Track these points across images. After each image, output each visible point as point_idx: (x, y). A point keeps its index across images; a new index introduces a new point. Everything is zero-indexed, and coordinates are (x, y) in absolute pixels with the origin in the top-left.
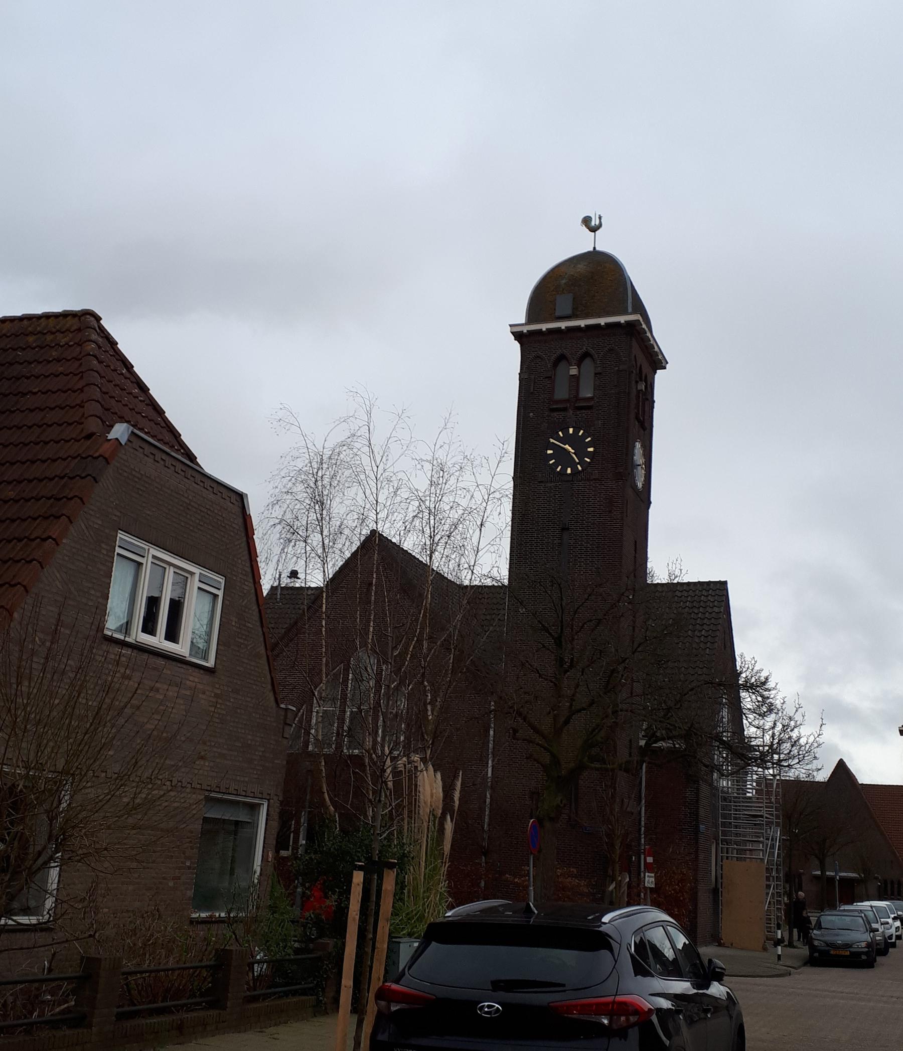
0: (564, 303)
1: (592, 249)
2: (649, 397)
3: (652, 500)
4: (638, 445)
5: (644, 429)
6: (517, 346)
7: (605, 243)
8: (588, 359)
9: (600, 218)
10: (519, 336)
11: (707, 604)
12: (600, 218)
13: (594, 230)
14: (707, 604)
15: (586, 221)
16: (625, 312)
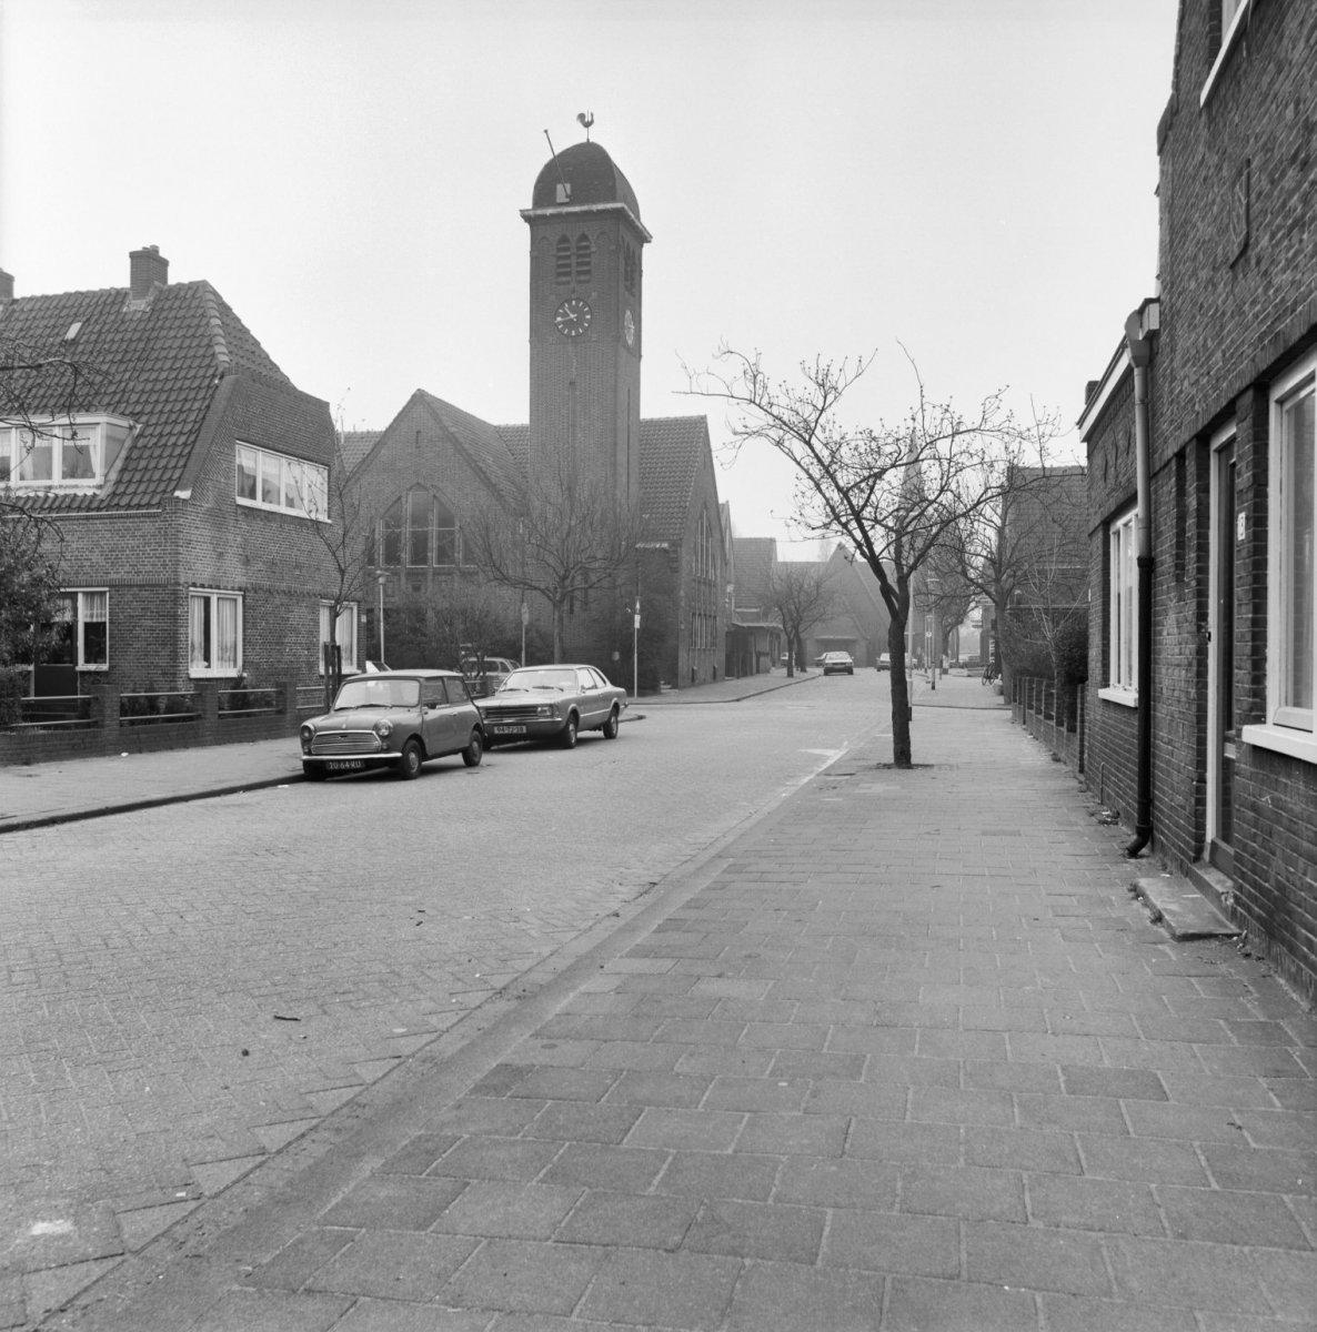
0: (562, 191)
1: (585, 141)
2: (637, 262)
3: (643, 353)
4: (628, 313)
5: (634, 296)
6: (527, 227)
7: (596, 136)
8: (585, 234)
9: (592, 115)
10: (527, 218)
11: (692, 433)
12: (592, 115)
13: (587, 125)
14: (692, 433)
15: (581, 117)
16: (614, 199)
